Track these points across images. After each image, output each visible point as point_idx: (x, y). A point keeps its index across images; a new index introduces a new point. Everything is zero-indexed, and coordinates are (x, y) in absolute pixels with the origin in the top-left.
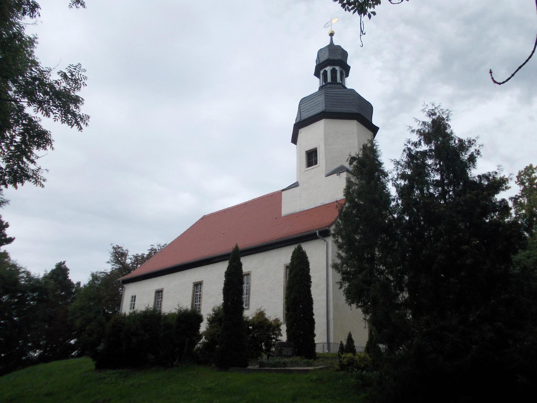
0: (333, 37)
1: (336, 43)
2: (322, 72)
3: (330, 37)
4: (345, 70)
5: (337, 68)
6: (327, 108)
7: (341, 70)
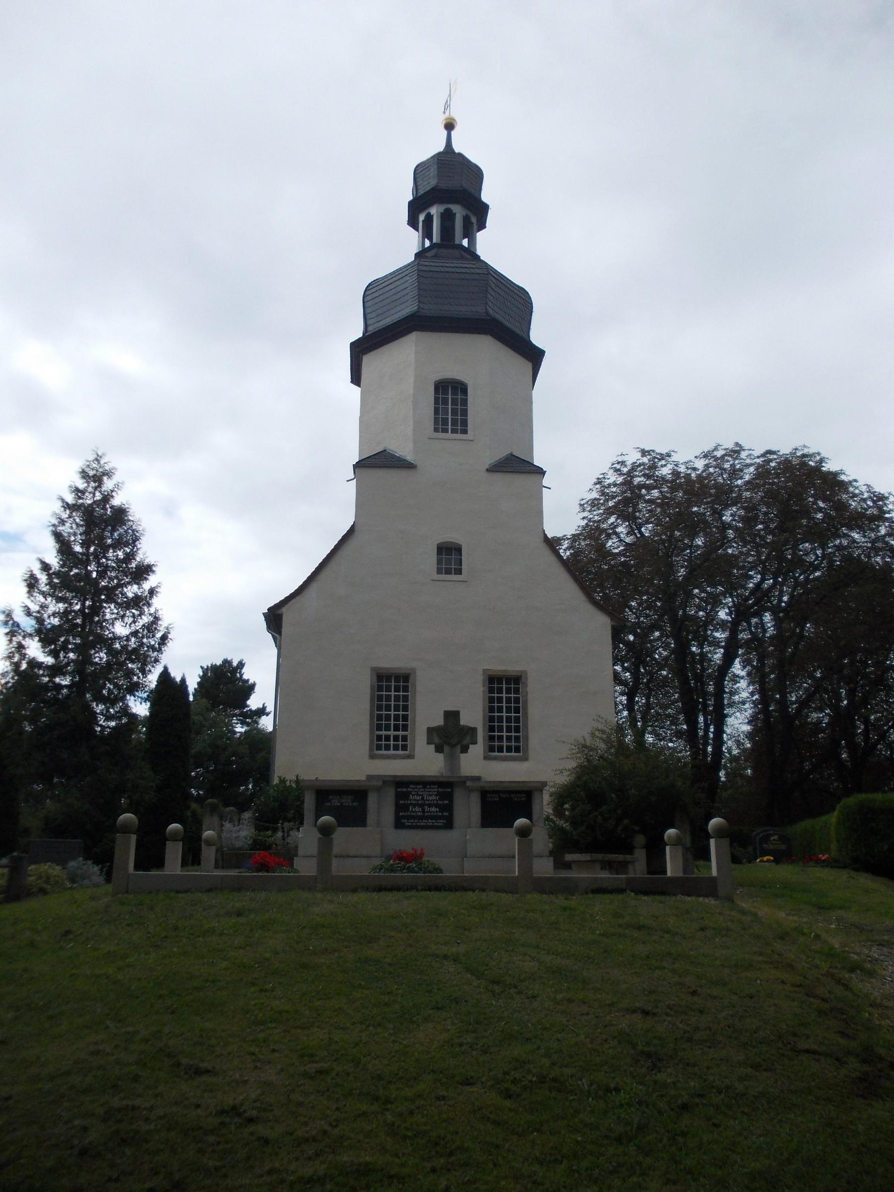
2: (422, 217)
3: (445, 133)
4: (475, 214)
5: (458, 211)
7: (466, 215)
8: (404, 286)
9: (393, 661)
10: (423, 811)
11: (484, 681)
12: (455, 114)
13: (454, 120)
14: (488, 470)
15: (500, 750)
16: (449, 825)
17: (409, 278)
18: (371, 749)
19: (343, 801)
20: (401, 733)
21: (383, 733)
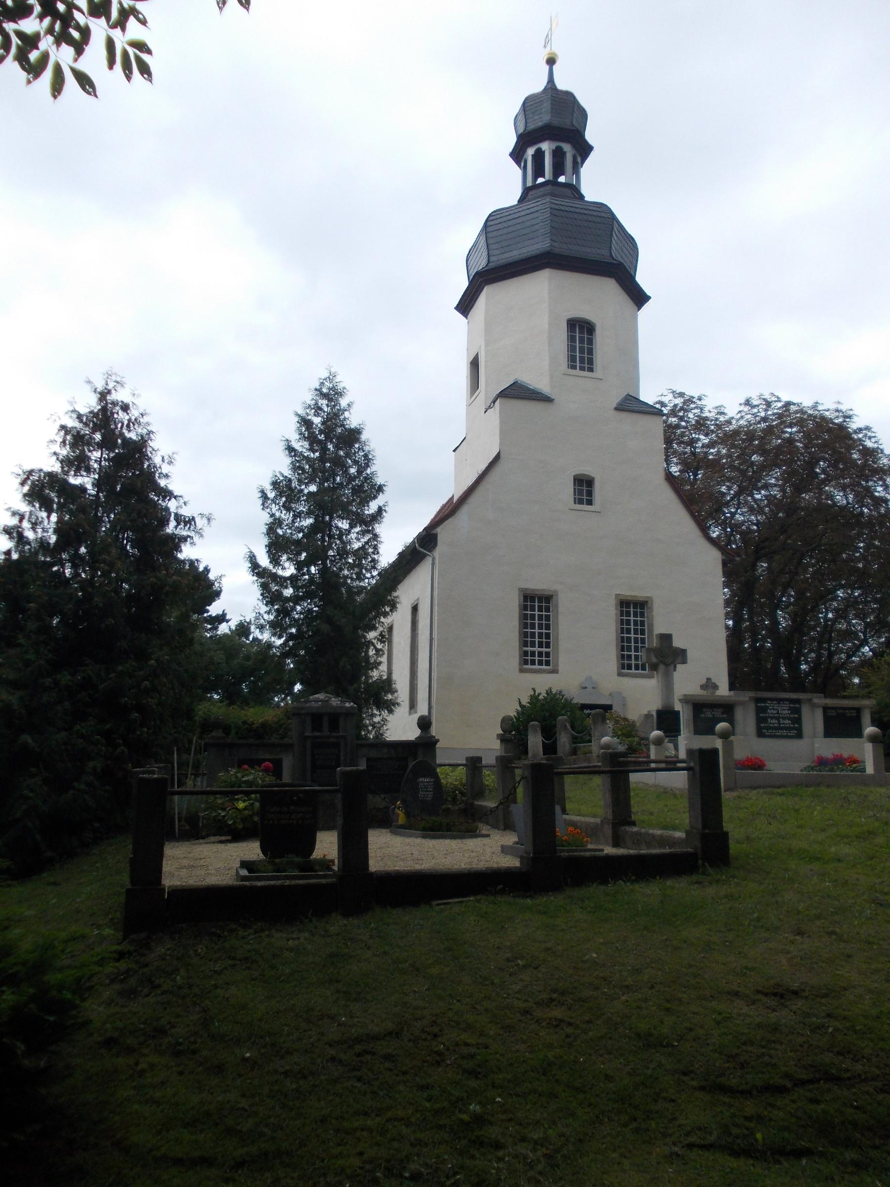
0: (554, 67)
1: (562, 85)
2: (531, 151)
3: (547, 68)
5: (567, 148)
6: (555, 244)
8: (534, 222)
9: (538, 583)
10: (779, 723)
11: (616, 605)
12: (557, 48)
13: (556, 55)
14: (616, 409)
15: (629, 667)
16: (799, 735)
17: (539, 214)
18: (520, 664)
19: (714, 713)
20: (544, 650)
21: (529, 649)
